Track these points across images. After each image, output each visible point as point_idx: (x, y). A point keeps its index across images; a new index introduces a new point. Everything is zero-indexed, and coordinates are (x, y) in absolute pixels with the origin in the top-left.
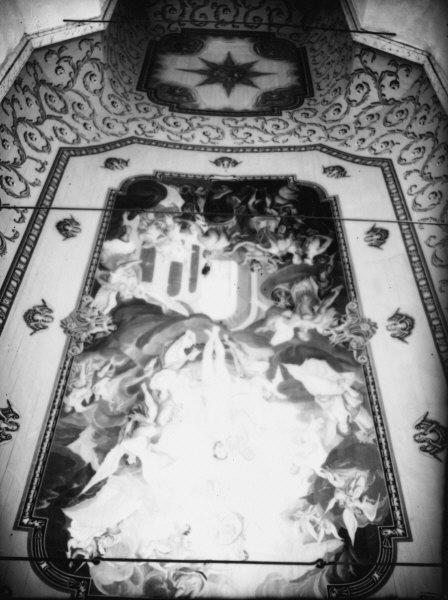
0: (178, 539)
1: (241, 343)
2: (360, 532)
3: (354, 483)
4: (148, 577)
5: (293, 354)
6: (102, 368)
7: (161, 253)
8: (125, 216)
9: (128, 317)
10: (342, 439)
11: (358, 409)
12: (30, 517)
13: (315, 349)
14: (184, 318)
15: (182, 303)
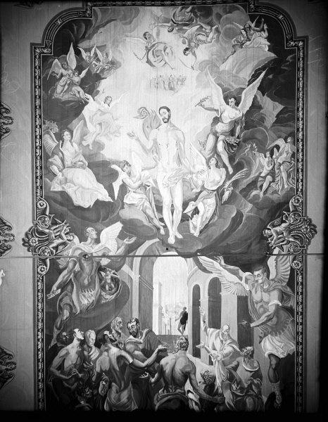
0: (193, 44)
1: (150, 225)
2: (66, 52)
3: (65, 89)
4: (210, 19)
5: (104, 212)
6: (269, 186)
7: (233, 341)
8: (278, 400)
9: (255, 247)
10: (69, 126)
11: (53, 154)
12: (298, 47)
13: (83, 218)
14: (203, 252)
15: (204, 270)
